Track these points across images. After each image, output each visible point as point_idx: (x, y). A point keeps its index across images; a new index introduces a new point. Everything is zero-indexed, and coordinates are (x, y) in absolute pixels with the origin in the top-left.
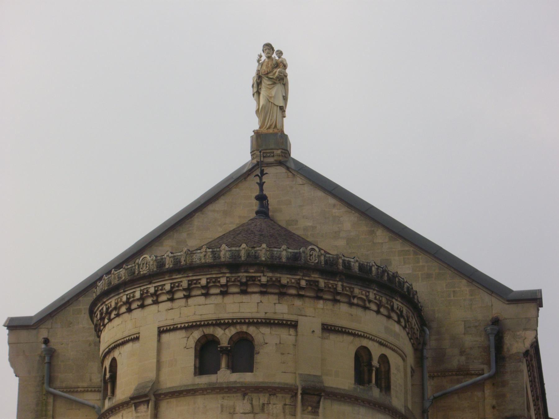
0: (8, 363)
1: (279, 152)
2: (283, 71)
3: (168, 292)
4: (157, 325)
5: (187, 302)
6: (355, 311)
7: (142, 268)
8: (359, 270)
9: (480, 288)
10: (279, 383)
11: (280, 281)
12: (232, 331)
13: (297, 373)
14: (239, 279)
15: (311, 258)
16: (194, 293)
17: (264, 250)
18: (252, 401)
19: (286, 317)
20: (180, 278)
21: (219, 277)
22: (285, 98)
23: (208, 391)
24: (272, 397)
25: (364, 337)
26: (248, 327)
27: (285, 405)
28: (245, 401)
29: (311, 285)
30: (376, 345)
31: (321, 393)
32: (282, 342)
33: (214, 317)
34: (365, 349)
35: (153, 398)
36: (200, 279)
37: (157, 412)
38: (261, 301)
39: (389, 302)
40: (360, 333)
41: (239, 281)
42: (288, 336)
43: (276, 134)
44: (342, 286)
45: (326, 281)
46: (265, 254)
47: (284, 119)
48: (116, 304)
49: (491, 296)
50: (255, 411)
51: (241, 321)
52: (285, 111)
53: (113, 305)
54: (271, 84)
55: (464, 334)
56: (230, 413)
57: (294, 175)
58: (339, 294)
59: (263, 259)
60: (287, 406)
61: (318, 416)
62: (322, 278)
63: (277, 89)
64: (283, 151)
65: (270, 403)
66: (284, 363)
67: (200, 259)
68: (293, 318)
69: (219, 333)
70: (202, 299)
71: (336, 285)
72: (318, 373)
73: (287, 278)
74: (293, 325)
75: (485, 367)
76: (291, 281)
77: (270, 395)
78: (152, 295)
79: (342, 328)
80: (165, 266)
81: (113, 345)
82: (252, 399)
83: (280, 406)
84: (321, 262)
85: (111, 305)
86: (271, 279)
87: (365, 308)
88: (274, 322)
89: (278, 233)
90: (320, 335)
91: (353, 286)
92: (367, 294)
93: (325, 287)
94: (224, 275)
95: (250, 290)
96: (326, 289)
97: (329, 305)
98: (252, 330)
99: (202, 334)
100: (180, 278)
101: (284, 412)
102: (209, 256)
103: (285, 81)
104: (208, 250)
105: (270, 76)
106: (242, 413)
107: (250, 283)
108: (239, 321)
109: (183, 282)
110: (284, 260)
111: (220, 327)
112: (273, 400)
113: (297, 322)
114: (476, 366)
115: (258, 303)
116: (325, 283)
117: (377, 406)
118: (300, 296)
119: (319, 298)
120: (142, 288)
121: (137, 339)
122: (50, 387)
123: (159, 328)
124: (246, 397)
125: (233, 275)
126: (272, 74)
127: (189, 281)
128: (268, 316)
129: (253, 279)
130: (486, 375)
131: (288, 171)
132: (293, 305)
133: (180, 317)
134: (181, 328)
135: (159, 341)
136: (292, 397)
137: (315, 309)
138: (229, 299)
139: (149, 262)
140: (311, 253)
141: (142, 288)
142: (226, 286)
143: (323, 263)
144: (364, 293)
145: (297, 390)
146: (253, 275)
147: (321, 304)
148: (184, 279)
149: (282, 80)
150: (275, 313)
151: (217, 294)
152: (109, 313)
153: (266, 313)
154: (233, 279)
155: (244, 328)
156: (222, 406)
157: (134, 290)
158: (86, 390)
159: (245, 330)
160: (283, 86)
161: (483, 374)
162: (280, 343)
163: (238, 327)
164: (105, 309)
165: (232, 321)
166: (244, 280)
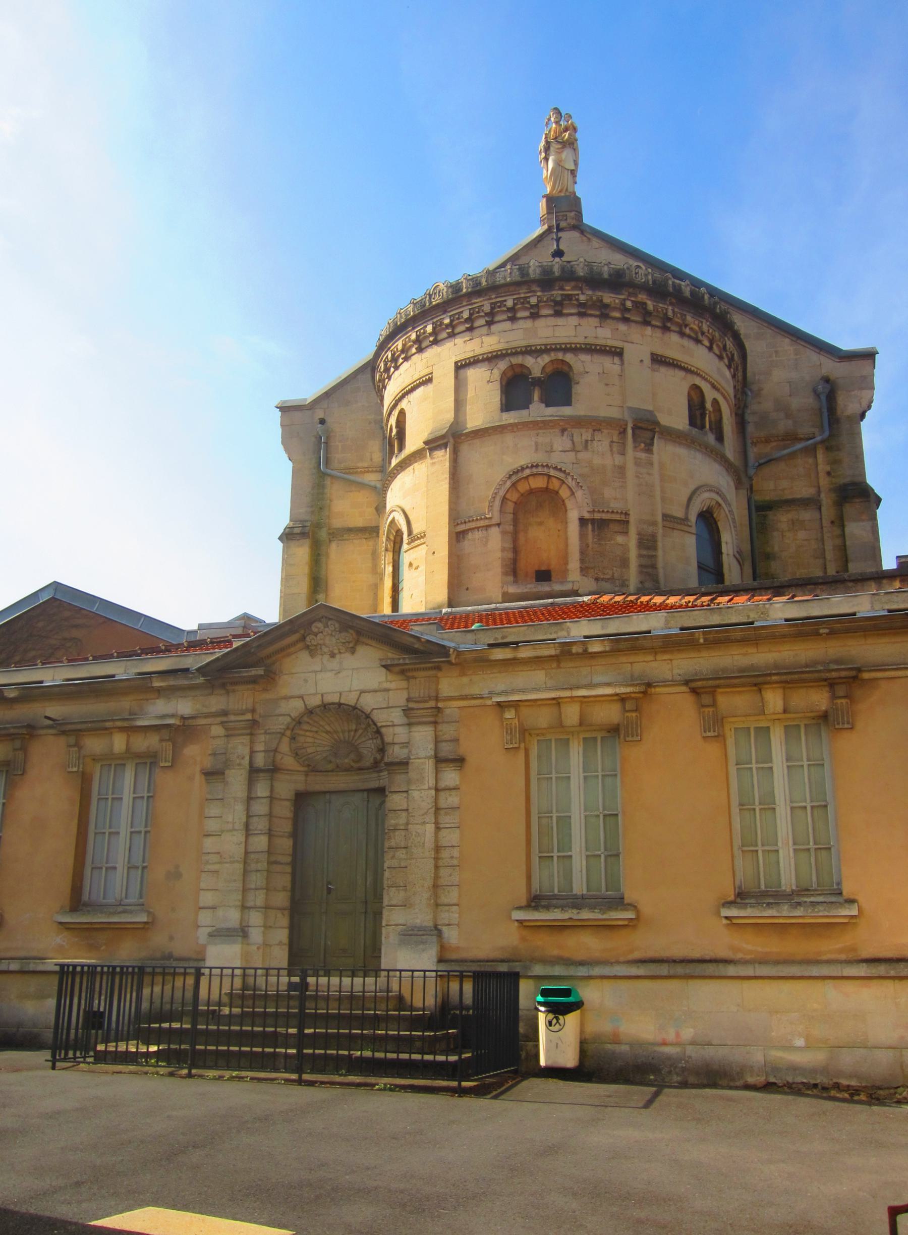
0: (281, 447)
1: (573, 214)
2: (574, 134)
3: (467, 320)
4: (454, 359)
5: (490, 329)
6: (686, 342)
7: (434, 299)
8: (691, 296)
9: (805, 346)
10: (604, 417)
11: (602, 301)
12: (546, 359)
13: (624, 406)
14: (552, 298)
15: (637, 276)
16: (497, 318)
17: (582, 264)
18: (573, 436)
19: (610, 343)
20: (481, 302)
21: (529, 297)
22: (576, 163)
23: (519, 427)
24: (596, 433)
25: (698, 375)
26: (564, 354)
27: (612, 442)
28: (564, 438)
29: (638, 307)
30: (709, 386)
31: (655, 429)
32: (605, 372)
33: (523, 343)
34: (696, 388)
35: (451, 440)
36: (505, 301)
37: (457, 456)
38: (579, 325)
39: (722, 340)
40: (692, 369)
41: (552, 301)
42: (612, 365)
43: (566, 197)
44: (673, 310)
45: (655, 304)
46: (583, 268)
47: (575, 186)
48: (404, 345)
49: (818, 355)
50: (577, 449)
51: (556, 347)
52: (576, 176)
53: (400, 347)
54: (561, 148)
55: (790, 396)
56: (547, 452)
57: (589, 239)
58: (670, 320)
59: (582, 274)
60: (615, 444)
61: (653, 454)
62: (650, 300)
63: (567, 154)
64: (577, 213)
65: (594, 440)
66: (608, 395)
67: (505, 278)
68: (618, 344)
69: (529, 361)
70: (507, 325)
71: (667, 309)
72: (650, 408)
73: (611, 297)
74: (618, 353)
75: (816, 430)
76: (615, 301)
77: (594, 430)
78: (447, 326)
79: (673, 360)
80: (462, 290)
81: (401, 394)
82: (573, 435)
83: (606, 443)
84: (648, 281)
85: (397, 349)
86: (591, 298)
87: (698, 341)
88: (596, 348)
89: (181, 1172)
90: (650, 366)
91: (685, 313)
92: (700, 324)
93: (654, 310)
94: (535, 294)
95: (565, 311)
96: (655, 314)
97: (658, 333)
98: (569, 357)
99: (510, 364)
100: (481, 302)
101: (611, 450)
102: (515, 273)
103: (575, 145)
104: (514, 267)
105: (560, 140)
106: (561, 451)
107: (565, 302)
108: (553, 347)
109: (485, 306)
110: (606, 276)
111: (530, 355)
112: (598, 436)
113: (623, 349)
114: (806, 429)
115: (576, 326)
116: (654, 306)
117: (714, 453)
118: (625, 320)
119: (646, 323)
120: (435, 320)
121: (430, 380)
122: (327, 468)
123: (456, 363)
124: (566, 433)
125: (546, 294)
126: (560, 138)
127: (491, 304)
128: (588, 341)
129: (569, 297)
130: (819, 438)
131: (581, 235)
132: (618, 329)
133: (482, 347)
134: (483, 360)
135: (456, 377)
136: (620, 433)
137: (642, 336)
138: (540, 323)
139: (443, 290)
140: (637, 271)
141: (435, 320)
142: (537, 306)
143: (651, 282)
144: (697, 322)
145: (626, 425)
146: (570, 292)
147: (649, 330)
148: (486, 302)
149: (571, 144)
150: (596, 338)
151: (525, 318)
152: (395, 359)
153: (586, 337)
154: (545, 299)
155: (560, 356)
156: (537, 444)
157: (425, 325)
158: (367, 471)
159: (561, 358)
160: (572, 151)
161: (814, 438)
162: (603, 373)
163: (552, 354)
164: (390, 356)
165: (546, 347)
166: (559, 299)
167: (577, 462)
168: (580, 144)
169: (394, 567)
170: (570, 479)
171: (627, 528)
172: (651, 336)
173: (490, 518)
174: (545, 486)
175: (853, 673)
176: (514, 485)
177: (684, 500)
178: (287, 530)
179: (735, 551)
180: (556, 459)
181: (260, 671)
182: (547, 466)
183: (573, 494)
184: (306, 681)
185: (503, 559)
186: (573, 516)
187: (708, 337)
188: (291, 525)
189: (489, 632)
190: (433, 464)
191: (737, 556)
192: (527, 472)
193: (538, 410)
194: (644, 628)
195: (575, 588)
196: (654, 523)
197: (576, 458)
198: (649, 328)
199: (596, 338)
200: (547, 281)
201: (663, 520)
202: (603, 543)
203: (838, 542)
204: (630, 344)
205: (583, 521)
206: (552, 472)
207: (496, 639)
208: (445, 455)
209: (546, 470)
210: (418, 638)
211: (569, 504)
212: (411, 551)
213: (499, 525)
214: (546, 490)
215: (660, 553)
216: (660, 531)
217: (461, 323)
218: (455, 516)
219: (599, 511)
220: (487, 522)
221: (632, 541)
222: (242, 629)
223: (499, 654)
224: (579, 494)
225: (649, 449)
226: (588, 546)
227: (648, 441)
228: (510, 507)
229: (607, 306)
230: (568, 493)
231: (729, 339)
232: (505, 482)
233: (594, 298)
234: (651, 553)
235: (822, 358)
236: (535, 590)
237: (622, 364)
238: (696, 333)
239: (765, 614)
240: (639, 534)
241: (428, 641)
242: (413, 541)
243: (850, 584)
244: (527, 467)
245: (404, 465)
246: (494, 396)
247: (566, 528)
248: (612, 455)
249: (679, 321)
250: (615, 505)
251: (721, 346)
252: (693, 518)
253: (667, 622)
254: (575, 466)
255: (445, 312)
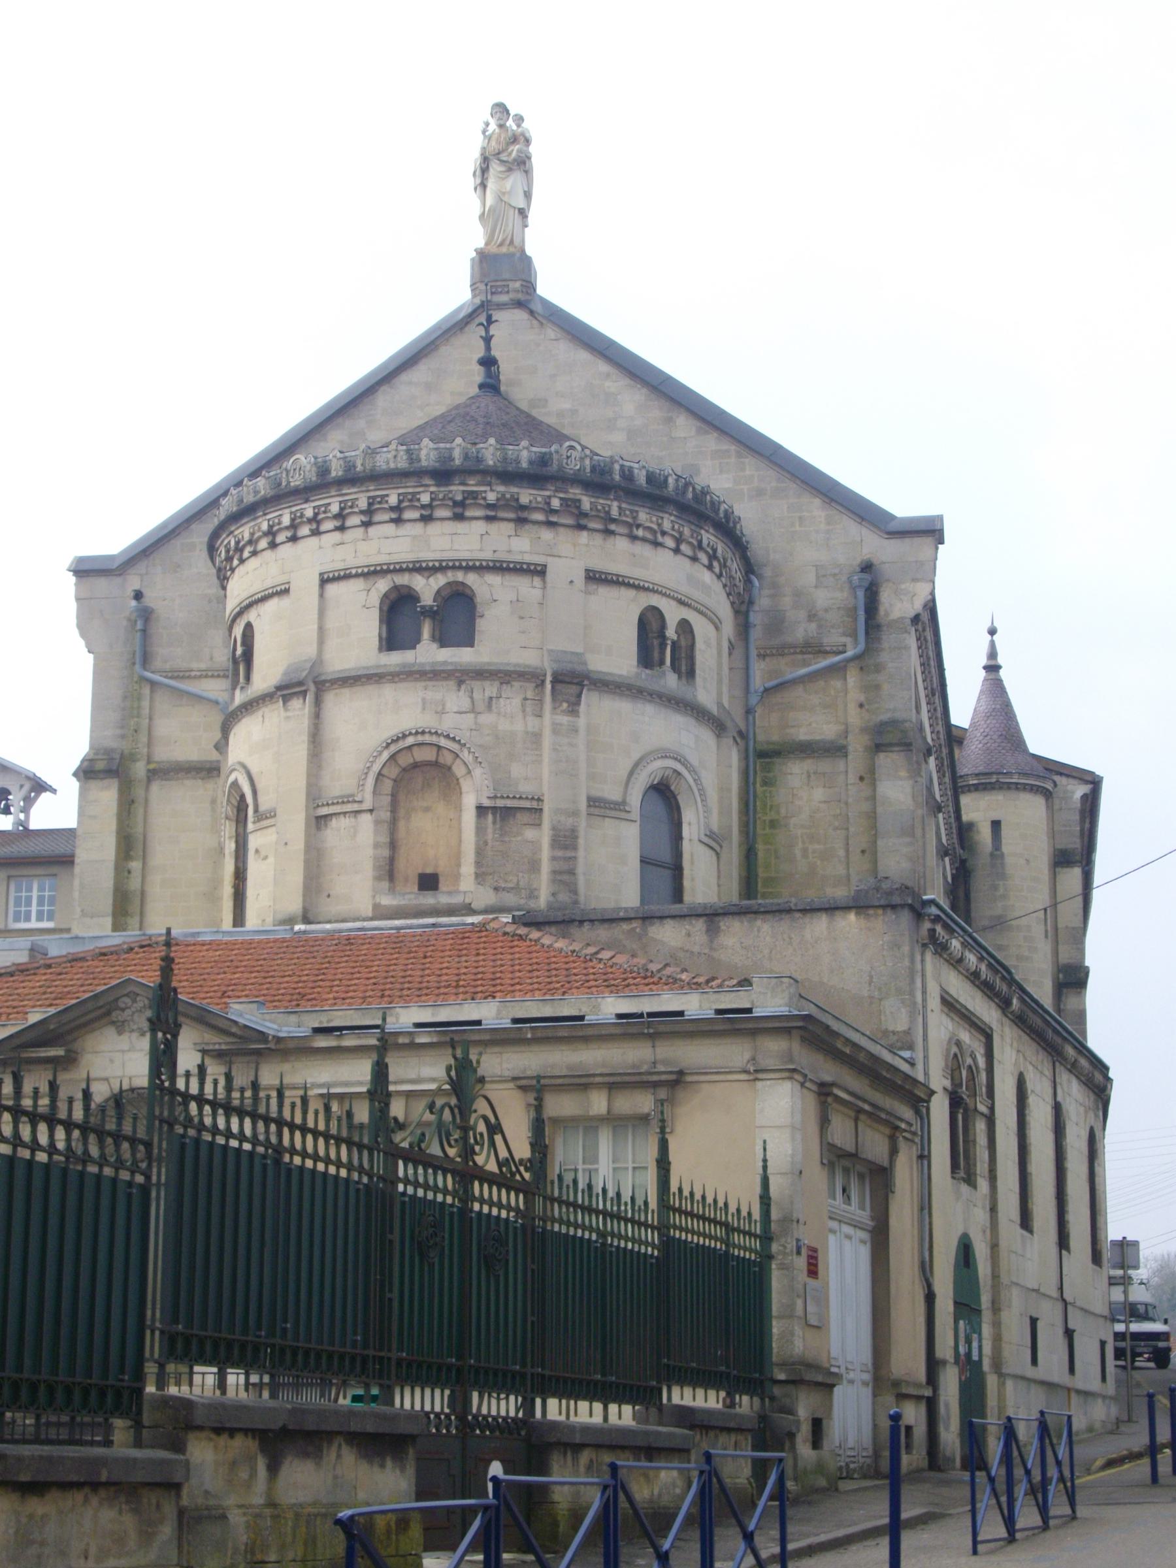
0: (76, 632)
1: (517, 285)
3: (336, 517)
11: (517, 500)
12: (439, 581)
19: (528, 558)
21: (419, 493)
22: (528, 195)
24: (504, 686)
27: (526, 699)
28: (462, 693)
29: (568, 506)
35: (312, 688)
36: (387, 495)
41: (450, 499)
43: (512, 255)
44: (620, 508)
53: (247, 536)
55: (816, 587)
56: (437, 712)
59: (491, 463)
60: (529, 702)
66: (523, 632)
68: (539, 559)
70: (390, 529)
71: (609, 506)
72: (580, 650)
74: (540, 571)
75: (848, 640)
83: (517, 701)
86: (503, 495)
87: (656, 544)
90: (583, 588)
95: (468, 513)
96: (594, 513)
97: (598, 539)
98: (471, 579)
101: (524, 711)
105: (504, 157)
112: (507, 691)
113: (545, 566)
114: (834, 638)
118: (550, 524)
119: (581, 527)
120: (294, 509)
121: (286, 591)
122: (145, 668)
123: (321, 574)
124: (463, 687)
126: (505, 154)
127: (369, 498)
129: (473, 495)
130: (849, 654)
134: (357, 576)
136: (537, 686)
137: (574, 545)
138: (434, 529)
141: (294, 509)
142: (430, 506)
144: (654, 519)
148: (361, 495)
149: (522, 164)
150: (509, 551)
152: (239, 550)
155: (460, 576)
156: (424, 700)
158: (205, 675)
164: (233, 543)
166: (459, 498)
167: (477, 728)
168: (537, 162)
169: (237, 842)
170: (466, 752)
171: (540, 819)
172: (587, 545)
173: (360, 802)
174: (434, 759)
175: (673, 1077)
176: (393, 757)
177: (624, 773)
178: (86, 764)
179: (702, 832)
180: (448, 724)
181: (60, 1052)
182: (436, 733)
183: (469, 772)
184: (112, 1061)
185: (376, 858)
186: (469, 801)
187: (672, 536)
188: (92, 756)
189: (314, 1015)
190: (288, 718)
191: (706, 840)
192: (410, 740)
193: (427, 652)
194: (474, 1017)
195: (467, 901)
196: (575, 813)
197: (476, 723)
198: (585, 534)
199: (509, 551)
200: (443, 474)
201: (589, 806)
202: (507, 839)
203: (865, 807)
204: (557, 559)
205: (481, 810)
206: (443, 742)
207: (321, 1022)
208: (303, 709)
209: (434, 739)
210: (235, 1022)
211: (466, 785)
212: (259, 833)
213: (371, 811)
214: (436, 764)
215: (581, 853)
216: (583, 823)
217: (327, 518)
218: (314, 796)
219: (502, 797)
220: (356, 807)
221: (544, 836)
222: (26, 953)
223: (322, 1042)
224: (477, 772)
225: (573, 710)
226: (486, 843)
227: (573, 699)
228: (388, 785)
229: (523, 508)
230: (463, 770)
231: (707, 531)
232: (380, 753)
233: (508, 496)
234: (569, 854)
235: (865, 531)
236: (414, 902)
237: (544, 588)
238: (654, 532)
239: (596, 1008)
240: (554, 828)
241: (246, 1026)
242: (259, 820)
243: (798, 915)
244: (410, 734)
245: (249, 707)
246: (369, 627)
247: (460, 816)
248: (525, 717)
249: (629, 520)
250: (526, 788)
251: (695, 543)
252: (635, 799)
253: (499, 1012)
254: (474, 733)
255: (307, 501)
